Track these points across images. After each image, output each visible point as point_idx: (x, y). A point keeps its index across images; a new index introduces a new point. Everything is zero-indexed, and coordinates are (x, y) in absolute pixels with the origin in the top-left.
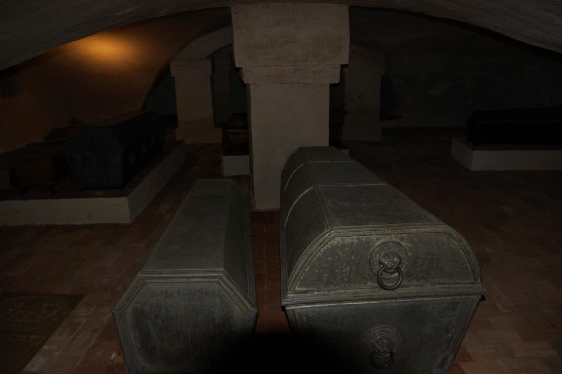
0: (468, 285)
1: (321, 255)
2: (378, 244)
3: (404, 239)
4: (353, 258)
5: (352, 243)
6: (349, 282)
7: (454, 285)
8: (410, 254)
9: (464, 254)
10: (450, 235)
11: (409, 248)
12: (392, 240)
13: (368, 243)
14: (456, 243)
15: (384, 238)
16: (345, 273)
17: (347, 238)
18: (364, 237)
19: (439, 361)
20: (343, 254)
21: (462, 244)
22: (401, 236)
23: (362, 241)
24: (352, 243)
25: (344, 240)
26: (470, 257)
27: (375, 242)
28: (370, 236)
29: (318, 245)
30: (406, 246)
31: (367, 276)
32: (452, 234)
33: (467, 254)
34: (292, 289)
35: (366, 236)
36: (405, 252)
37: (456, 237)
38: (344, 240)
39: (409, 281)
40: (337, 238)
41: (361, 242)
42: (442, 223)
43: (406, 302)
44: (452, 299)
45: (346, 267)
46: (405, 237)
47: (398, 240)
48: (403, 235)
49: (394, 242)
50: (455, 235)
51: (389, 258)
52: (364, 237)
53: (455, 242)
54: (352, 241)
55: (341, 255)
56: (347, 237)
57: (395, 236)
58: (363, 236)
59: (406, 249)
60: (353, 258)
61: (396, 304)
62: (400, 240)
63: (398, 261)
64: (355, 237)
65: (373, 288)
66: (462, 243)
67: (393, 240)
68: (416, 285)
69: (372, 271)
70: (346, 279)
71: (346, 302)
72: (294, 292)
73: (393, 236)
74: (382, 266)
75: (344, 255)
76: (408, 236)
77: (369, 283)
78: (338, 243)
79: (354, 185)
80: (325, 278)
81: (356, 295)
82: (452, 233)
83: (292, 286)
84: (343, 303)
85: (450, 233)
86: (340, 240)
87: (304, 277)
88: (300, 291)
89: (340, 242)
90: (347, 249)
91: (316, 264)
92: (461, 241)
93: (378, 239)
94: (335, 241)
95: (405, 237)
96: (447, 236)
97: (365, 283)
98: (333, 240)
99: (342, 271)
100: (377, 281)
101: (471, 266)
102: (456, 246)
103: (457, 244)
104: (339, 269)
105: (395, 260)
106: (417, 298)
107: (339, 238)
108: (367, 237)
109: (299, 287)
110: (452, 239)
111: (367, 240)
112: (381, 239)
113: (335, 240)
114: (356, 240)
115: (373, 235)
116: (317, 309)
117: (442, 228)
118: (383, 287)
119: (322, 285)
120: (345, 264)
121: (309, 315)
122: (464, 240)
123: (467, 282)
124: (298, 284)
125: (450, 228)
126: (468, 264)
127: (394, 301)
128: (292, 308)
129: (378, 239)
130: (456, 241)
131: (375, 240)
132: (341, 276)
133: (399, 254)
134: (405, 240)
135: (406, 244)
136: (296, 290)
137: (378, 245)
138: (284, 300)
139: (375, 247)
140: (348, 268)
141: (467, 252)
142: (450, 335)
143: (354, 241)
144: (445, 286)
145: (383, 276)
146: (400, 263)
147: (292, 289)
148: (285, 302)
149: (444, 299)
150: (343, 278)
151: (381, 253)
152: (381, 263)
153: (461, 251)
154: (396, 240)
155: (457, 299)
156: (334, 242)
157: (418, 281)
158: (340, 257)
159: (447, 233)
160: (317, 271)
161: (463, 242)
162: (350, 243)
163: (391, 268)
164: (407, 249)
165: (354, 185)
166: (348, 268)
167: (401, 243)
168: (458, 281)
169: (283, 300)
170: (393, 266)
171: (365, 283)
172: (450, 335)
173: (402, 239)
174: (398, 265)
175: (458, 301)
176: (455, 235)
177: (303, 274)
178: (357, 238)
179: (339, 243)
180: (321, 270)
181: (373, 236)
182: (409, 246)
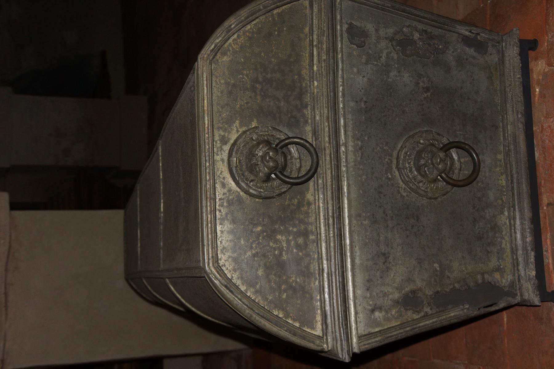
0: (315, 10)
1: (252, 290)
2: (233, 184)
3: (223, 137)
4: (259, 228)
5: (230, 232)
6: (305, 234)
7: (315, 37)
8: (254, 124)
9: (255, 22)
10: (215, 51)
11: (241, 126)
12: (226, 158)
13: (230, 203)
14: (233, 38)
15: (221, 173)
16: (288, 242)
17: (221, 242)
18: (220, 211)
19: (471, 51)
20: (251, 248)
21: (234, 27)
22: (218, 142)
23: (227, 214)
24: (230, 232)
25: (224, 248)
26: (260, 10)
27: (230, 190)
28: (217, 200)
29: (234, 296)
30: (238, 131)
31: (295, 201)
32: (215, 47)
33: (254, 16)
34: (318, 342)
35: (217, 207)
36: (248, 133)
37: (220, 39)
38: (224, 248)
39: (306, 122)
40: (219, 262)
41: (229, 215)
42: (196, 63)
43: (345, 126)
44: (342, 39)
45: (276, 241)
46: (220, 135)
47: (227, 148)
48: (217, 138)
49: (230, 155)
50: (217, 41)
51: (258, 165)
52: (220, 211)
53: (230, 41)
54: (225, 232)
55: (254, 252)
56: (219, 243)
57: (219, 153)
58: (217, 212)
59: (244, 132)
60: (259, 228)
61: (351, 144)
62: (225, 143)
63: (263, 147)
64: (219, 228)
65: (317, 190)
66: (233, 26)
67: (225, 156)
68: (313, 109)
69: (284, 193)
70: (301, 240)
71: (345, 239)
72: (325, 337)
73: (217, 158)
74: (273, 176)
75: (254, 246)
76: (219, 128)
77: (309, 197)
78: (230, 260)
79: (162, 201)
80: (298, 280)
81: (331, 221)
82: (213, 46)
83: (313, 343)
84: (345, 245)
85: (213, 49)
86: (224, 254)
87: (295, 320)
88: (322, 325)
89: (228, 254)
90: (242, 242)
91: (270, 298)
92: (229, 30)
93: (224, 185)
94: (227, 264)
95: (220, 135)
96: (219, 55)
97: (309, 204)
98: (224, 268)
99: (285, 248)
100: (307, 184)
101: (278, 7)
102: (239, 37)
103: (235, 36)
104: (281, 254)
105: (260, 154)
106: (340, 106)
107: (220, 257)
108: (219, 205)
109: (313, 328)
110: (226, 45)
111: (225, 204)
112: (224, 178)
113: (225, 265)
114: (224, 226)
115: (215, 194)
116: (359, 292)
117: (203, 67)
118: (313, 173)
119: (312, 285)
120: (271, 244)
121: (370, 308)
122: (226, 24)
123: (308, 11)
124: (308, 330)
125: (203, 52)
126: (275, 12)
127: (343, 149)
128: (355, 340)
129: (224, 185)
130: (229, 38)
131: (225, 191)
132: (295, 250)
133: (251, 145)
134: (226, 134)
135: (235, 131)
136: (321, 335)
137: (236, 183)
138: (341, 356)
139: (239, 190)
140: (279, 237)
141: (252, 15)
142: (416, 36)
143: (227, 229)
144: (315, 53)
145: (293, 172)
146: (268, 143)
147: (318, 342)
148: (343, 355)
149: (342, 55)
150: (298, 246)
151: (250, 180)
152: (268, 179)
153: (249, 27)
154: (227, 152)
155: (341, 30)
156: (227, 266)
157: (306, 107)
158: (257, 253)
159: (214, 58)
160: (284, 296)
161: (231, 25)
162: (231, 237)
163: (275, 161)
164: (244, 129)
165: (162, 201)
166: (279, 237)
167: (232, 142)
168: (307, 30)
169: (340, 358)
170: (270, 158)
171: (309, 204)
172: (416, 36)
173: (224, 141)
174: (271, 148)
175: (345, 27)
176: (217, 41)
177: (291, 322)
178: (221, 224)
179: (229, 257)
180: (283, 287)
181: (217, 194)
182: (238, 125)
